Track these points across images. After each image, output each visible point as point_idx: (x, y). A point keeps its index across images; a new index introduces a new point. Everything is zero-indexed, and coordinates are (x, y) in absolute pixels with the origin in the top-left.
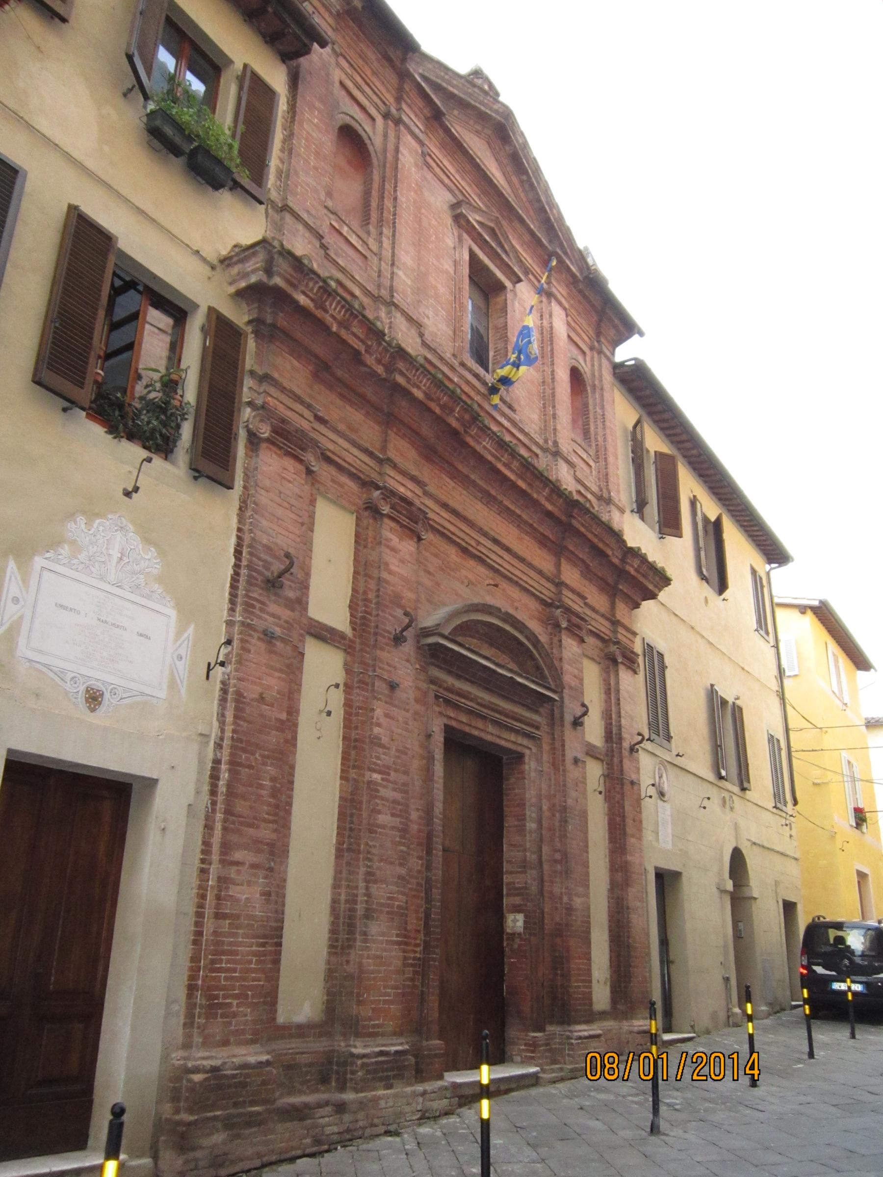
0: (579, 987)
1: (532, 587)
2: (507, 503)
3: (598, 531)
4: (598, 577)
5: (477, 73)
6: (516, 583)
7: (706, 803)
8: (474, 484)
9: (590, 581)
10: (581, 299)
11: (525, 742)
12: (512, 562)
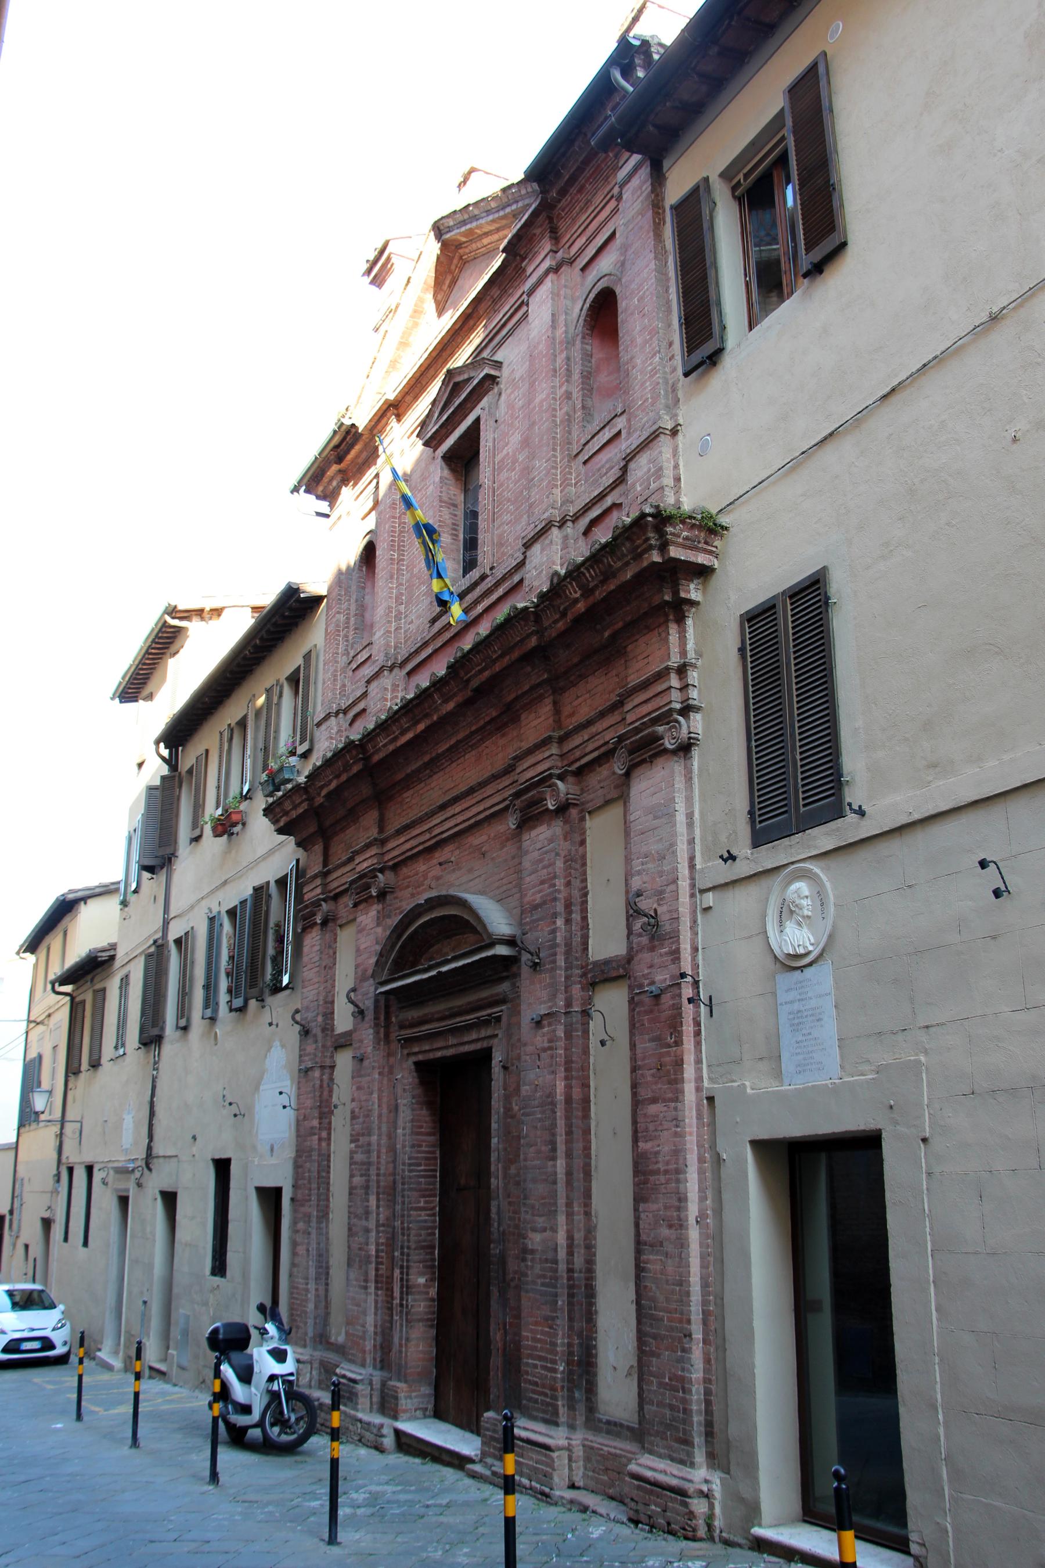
0: (535, 1366)
1: (456, 825)
2: (442, 748)
3: (496, 650)
4: (581, 662)
5: (439, 229)
6: (478, 824)
7: (991, 878)
8: (418, 771)
9: (582, 677)
10: (573, 190)
11: (483, 1033)
12: (449, 814)
